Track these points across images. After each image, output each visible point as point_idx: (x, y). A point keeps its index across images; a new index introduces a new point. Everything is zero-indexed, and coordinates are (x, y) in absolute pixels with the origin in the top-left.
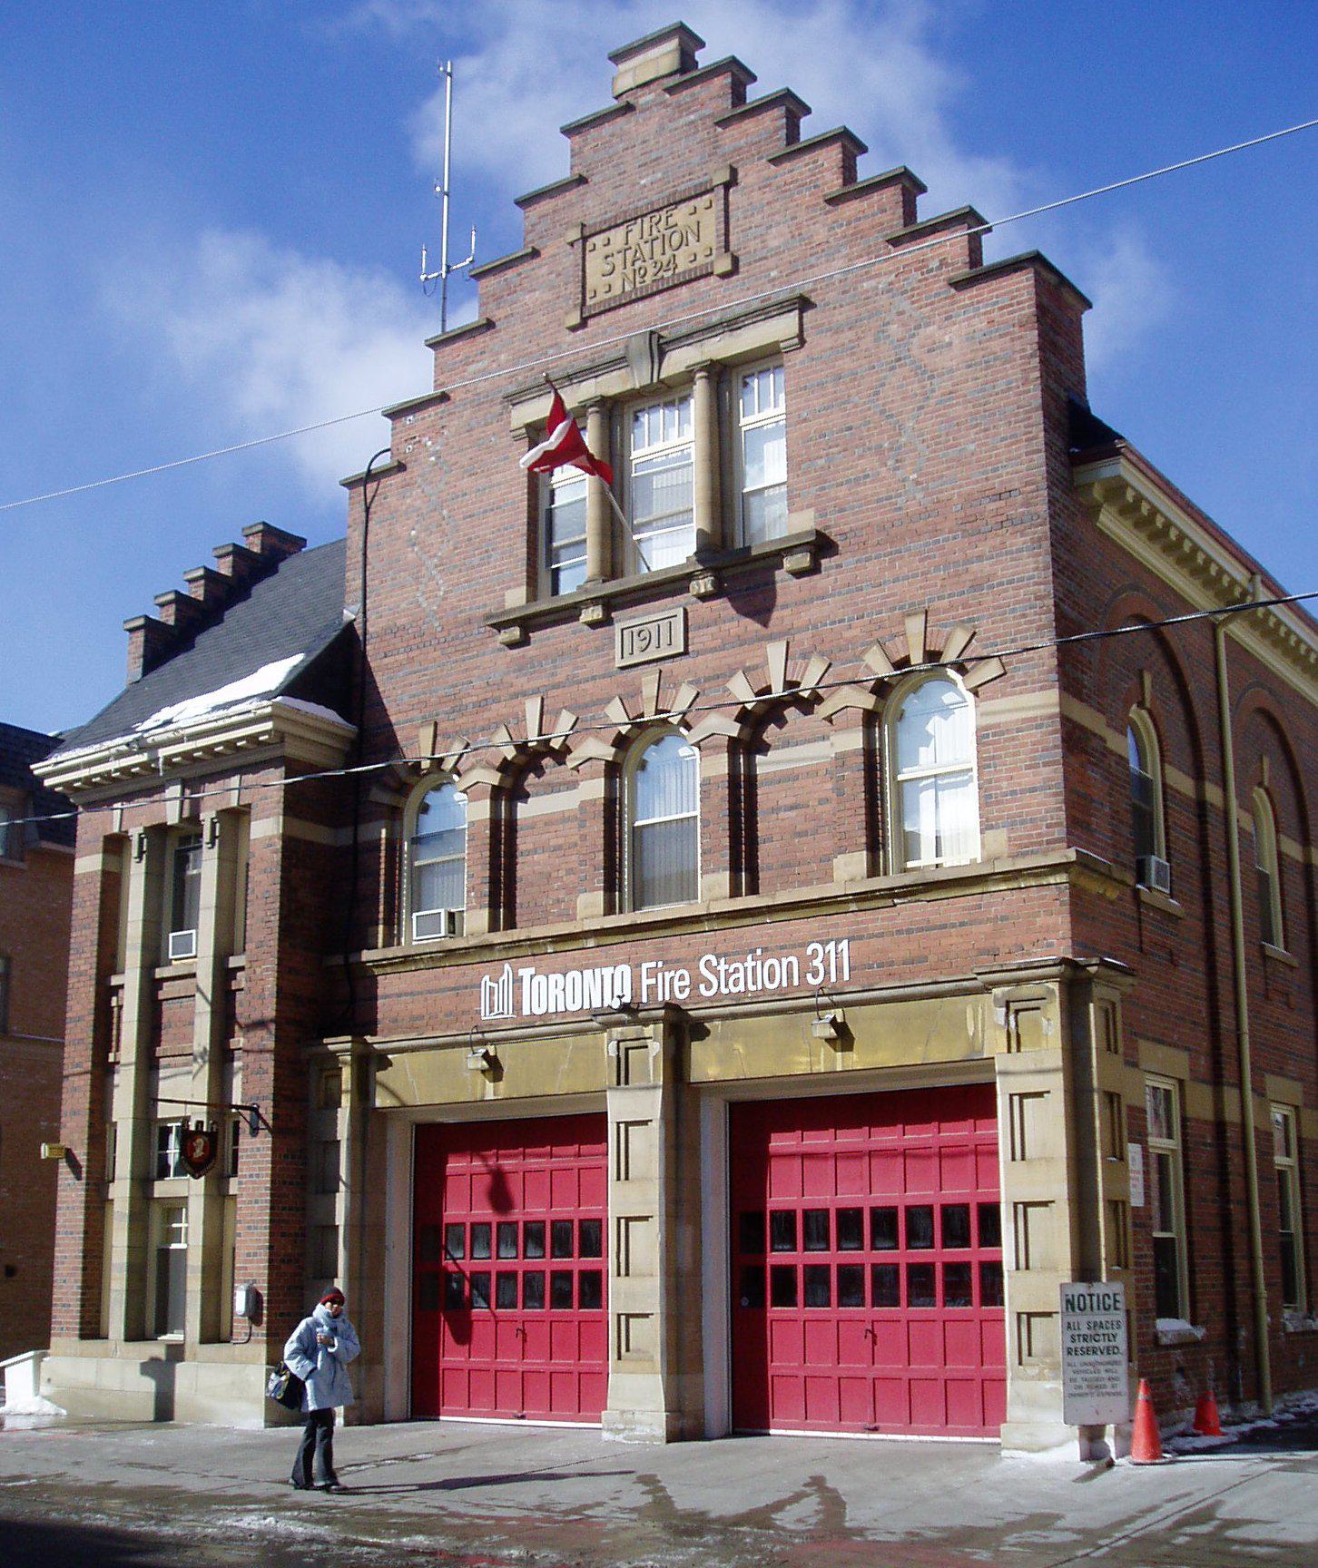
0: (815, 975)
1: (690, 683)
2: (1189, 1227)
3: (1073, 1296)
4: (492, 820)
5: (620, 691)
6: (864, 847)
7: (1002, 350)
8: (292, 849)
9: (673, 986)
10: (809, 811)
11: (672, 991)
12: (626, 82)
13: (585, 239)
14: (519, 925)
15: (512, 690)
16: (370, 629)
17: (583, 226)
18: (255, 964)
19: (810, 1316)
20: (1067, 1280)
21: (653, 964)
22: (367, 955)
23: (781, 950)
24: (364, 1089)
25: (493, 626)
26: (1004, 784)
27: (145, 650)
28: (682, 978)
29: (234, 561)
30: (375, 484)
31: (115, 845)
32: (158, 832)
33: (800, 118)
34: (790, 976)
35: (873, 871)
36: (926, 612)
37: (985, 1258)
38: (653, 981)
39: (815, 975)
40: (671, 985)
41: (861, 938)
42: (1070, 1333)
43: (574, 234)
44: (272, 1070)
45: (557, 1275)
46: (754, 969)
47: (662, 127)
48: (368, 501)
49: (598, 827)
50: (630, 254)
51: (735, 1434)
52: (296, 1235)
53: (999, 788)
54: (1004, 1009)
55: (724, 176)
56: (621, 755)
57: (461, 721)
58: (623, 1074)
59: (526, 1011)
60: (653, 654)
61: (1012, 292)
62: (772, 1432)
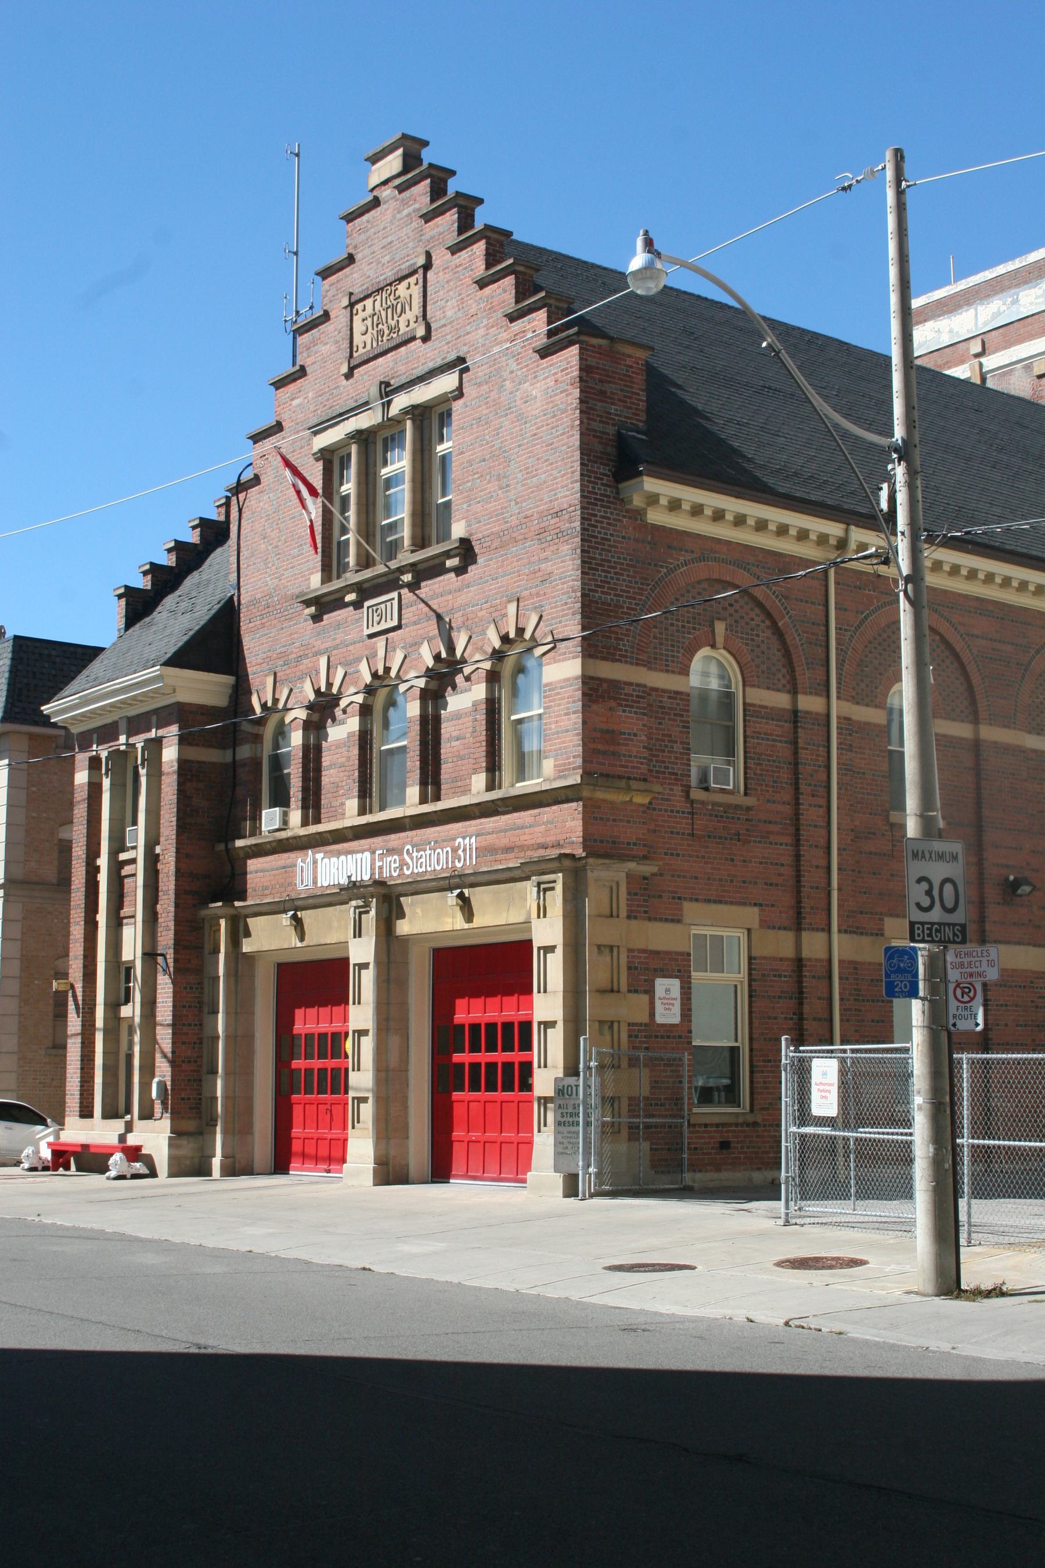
0: (459, 861)
1: (402, 647)
2: (751, 1039)
3: (564, 1086)
4: (304, 745)
5: (367, 652)
6: (484, 769)
7: (562, 403)
8: (184, 766)
9: (390, 868)
10: (466, 741)
11: (390, 871)
12: (374, 180)
13: (351, 305)
14: (323, 821)
15: (314, 650)
16: (243, 602)
17: (351, 294)
18: (165, 852)
19: (472, 1098)
20: (561, 1075)
21: (381, 852)
22: (239, 843)
23: (438, 843)
24: (235, 942)
25: (303, 602)
26: (553, 726)
27: (126, 611)
28: (395, 861)
29: (201, 531)
30: (245, 493)
31: (95, 763)
32: (115, 755)
33: (473, 210)
34: (447, 863)
35: (491, 786)
36: (518, 600)
37: (489, 1060)
38: (381, 864)
39: (459, 861)
40: (390, 867)
41: (483, 834)
42: (561, 1111)
43: (345, 302)
44: (173, 928)
45: (322, 1071)
46: (430, 855)
47: (394, 216)
48: (241, 504)
49: (482, 717)
50: (376, 318)
51: (433, 1182)
52: (195, 1043)
53: (551, 729)
54: (536, 889)
55: (421, 261)
56: (371, 698)
57: (288, 672)
58: (358, 933)
59: (319, 885)
60: (384, 626)
61: (567, 358)
62: (451, 1181)
